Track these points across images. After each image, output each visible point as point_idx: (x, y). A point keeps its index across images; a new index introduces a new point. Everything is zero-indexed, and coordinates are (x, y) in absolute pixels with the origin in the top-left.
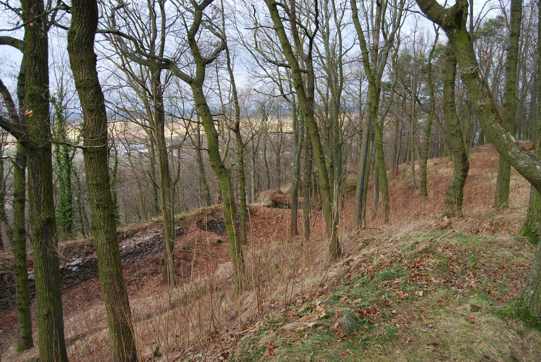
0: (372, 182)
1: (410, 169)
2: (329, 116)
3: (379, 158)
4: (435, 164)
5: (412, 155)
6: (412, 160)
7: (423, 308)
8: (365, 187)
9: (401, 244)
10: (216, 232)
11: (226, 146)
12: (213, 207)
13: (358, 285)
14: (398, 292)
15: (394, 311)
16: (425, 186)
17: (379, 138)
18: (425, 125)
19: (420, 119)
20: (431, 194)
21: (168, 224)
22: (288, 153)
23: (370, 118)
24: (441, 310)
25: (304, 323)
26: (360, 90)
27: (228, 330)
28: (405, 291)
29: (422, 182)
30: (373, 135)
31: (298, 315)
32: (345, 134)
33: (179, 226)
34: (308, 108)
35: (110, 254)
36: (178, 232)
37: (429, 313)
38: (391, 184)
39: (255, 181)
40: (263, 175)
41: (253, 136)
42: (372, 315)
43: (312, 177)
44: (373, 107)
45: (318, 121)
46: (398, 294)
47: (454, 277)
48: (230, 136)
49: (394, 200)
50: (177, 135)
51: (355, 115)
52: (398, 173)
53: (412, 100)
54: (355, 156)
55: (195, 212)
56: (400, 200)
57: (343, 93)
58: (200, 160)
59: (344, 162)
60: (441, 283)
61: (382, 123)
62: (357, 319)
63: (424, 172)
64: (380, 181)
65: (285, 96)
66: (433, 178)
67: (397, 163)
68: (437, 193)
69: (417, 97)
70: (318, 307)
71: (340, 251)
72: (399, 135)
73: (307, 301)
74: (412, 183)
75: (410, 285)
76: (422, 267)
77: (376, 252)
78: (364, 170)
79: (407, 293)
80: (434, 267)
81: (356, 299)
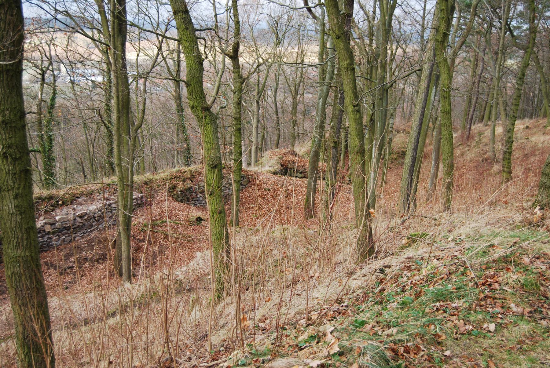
0: (430, 148)
1: (488, 133)
2: (374, 46)
3: (443, 112)
4: (527, 127)
5: (493, 112)
6: (493, 119)
7: (493, 351)
8: (418, 154)
9: (467, 245)
10: (195, 205)
11: (218, 79)
12: (193, 167)
13: (394, 305)
14: (457, 322)
15: (447, 353)
16: (509, 159)
17: (446, 82)
18: (515, 67)
19: (511, 58)
20: (518, 171)
21: (124, 189)
22: (310, 96)
23: (435, 49)
24: (522, 357)
25: (305, 360)
26: (424, 9)
27: (190, 359)
28: (466, 322)
29: (505, 152)
30: (438, 77)
31: (297, 345)
32: (396, 74)
33: (141, 192)
34: (340, 27)
35: (21, 230)
36: (139, 202)
37: (502, 360)
38: (458, 152)
39: (257, 134)
40: (270, 127)
41: (258, 67)
42: (412, 355)
43: (343, 134)
44: (441, 34)
45: (357, 52)
46: (455, 326)
47: (545, 305)
48: (224, 64)
49: (461, 176)
50: (147, 57)
51: (412, 48)
52: (469, 137)
53: (500, 29)
54: (409, 108)
55: (166, 174)
56: (470, 176)
57: (397, 12)
58: (178, 98)
59: (392, 115)
60: (526, 312)
61: (453, 60)
62: (387, 361)
63: (510, 138)
64: (442, 147)
65: (309, 10)
66: (521, 148)
67: (469, 123)
68: (527, 170)
69: (509, 25)
70: (329, 336)
71: (373, 248)
72: (477, 81)
73: (314, 323)
74: (490, 154)
75: (476, 312)
76: (496, 286)
77: (427, 255)
78: (420, 129)
79: (470, 324)
80: (516, 286)
81: (389, 327)
